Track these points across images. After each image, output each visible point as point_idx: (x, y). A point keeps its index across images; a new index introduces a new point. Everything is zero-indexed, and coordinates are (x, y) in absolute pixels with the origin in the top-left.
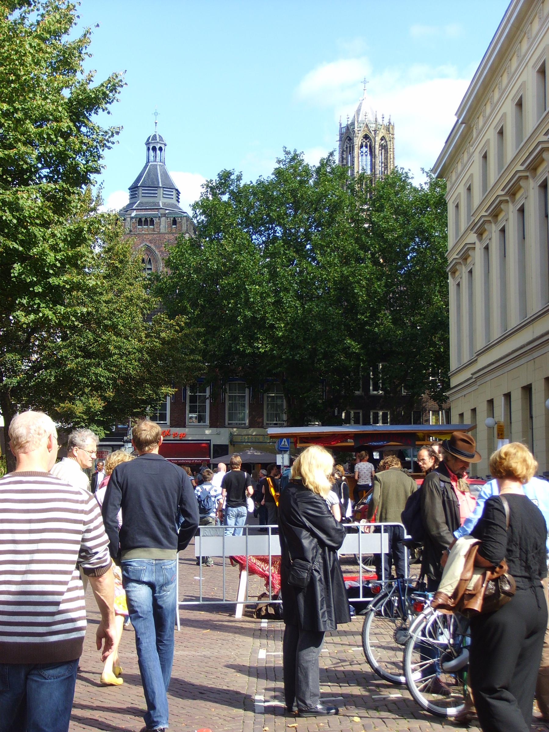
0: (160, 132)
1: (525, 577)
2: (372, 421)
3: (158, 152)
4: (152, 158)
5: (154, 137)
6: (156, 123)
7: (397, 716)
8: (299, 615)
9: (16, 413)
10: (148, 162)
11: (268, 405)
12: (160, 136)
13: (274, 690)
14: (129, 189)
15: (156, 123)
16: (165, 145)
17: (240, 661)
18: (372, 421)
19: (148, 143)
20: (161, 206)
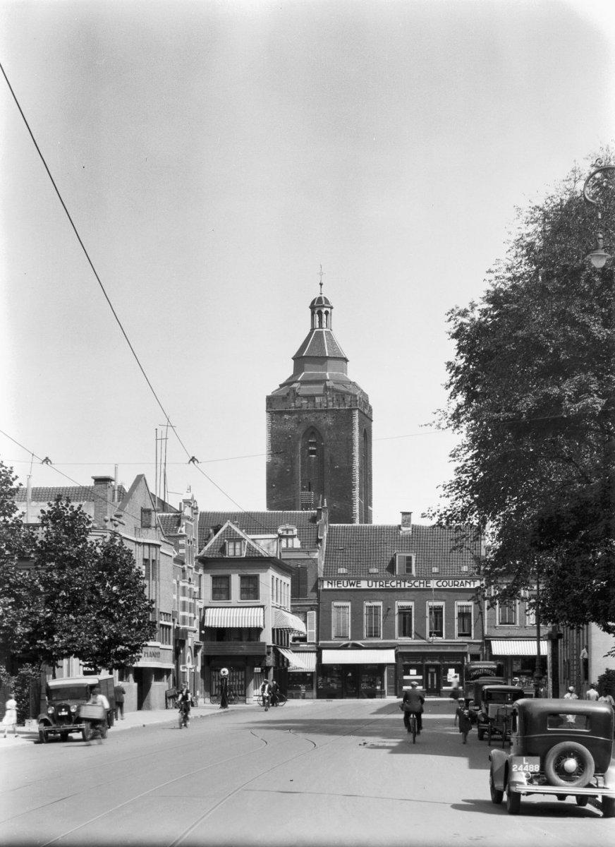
0: (326, 294)
1: (477, 677)
2: (365, 634)
3: (324, 316)
4: (317, 325)
5: (320, 299)
6: (321, 284)
7: (284, 561)
8: (468, 805)
9: (72, 655)
10: (313, 329)
11: (216, 687)
12: (325, 298)
13: (344, 628)
14: (293, 359)
15: (321, 284)
16: (332, 308)
17: (372, 712)
18: (365, 634)
19: (312, 307)
20: (327, 355)
